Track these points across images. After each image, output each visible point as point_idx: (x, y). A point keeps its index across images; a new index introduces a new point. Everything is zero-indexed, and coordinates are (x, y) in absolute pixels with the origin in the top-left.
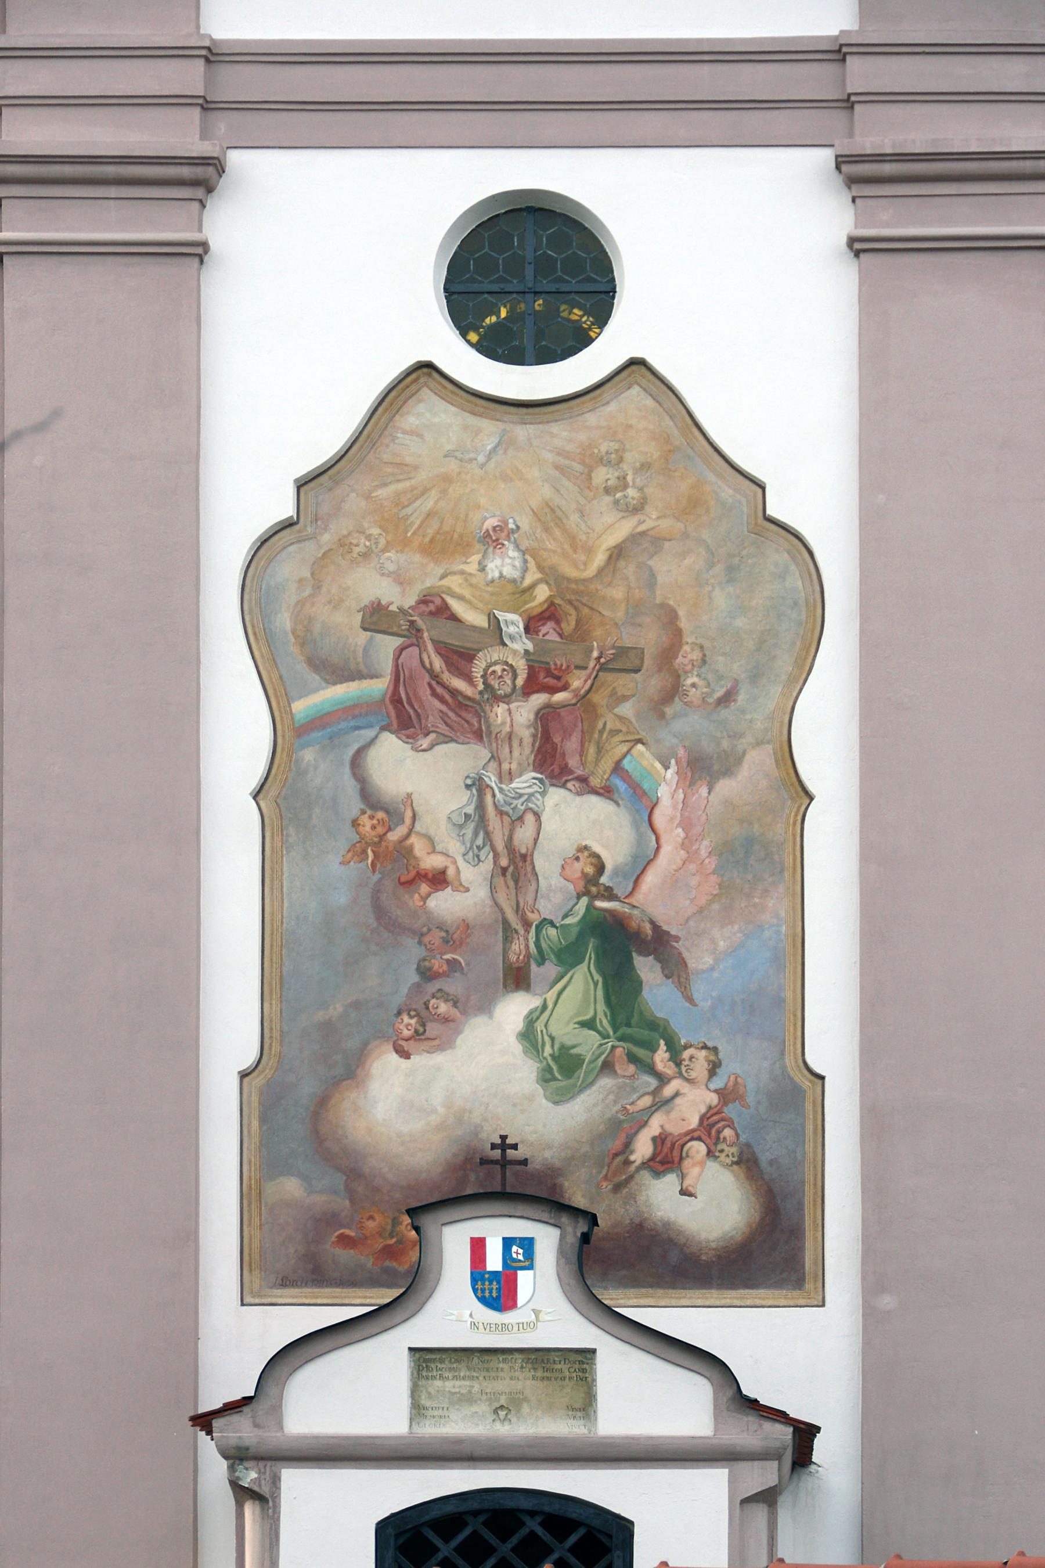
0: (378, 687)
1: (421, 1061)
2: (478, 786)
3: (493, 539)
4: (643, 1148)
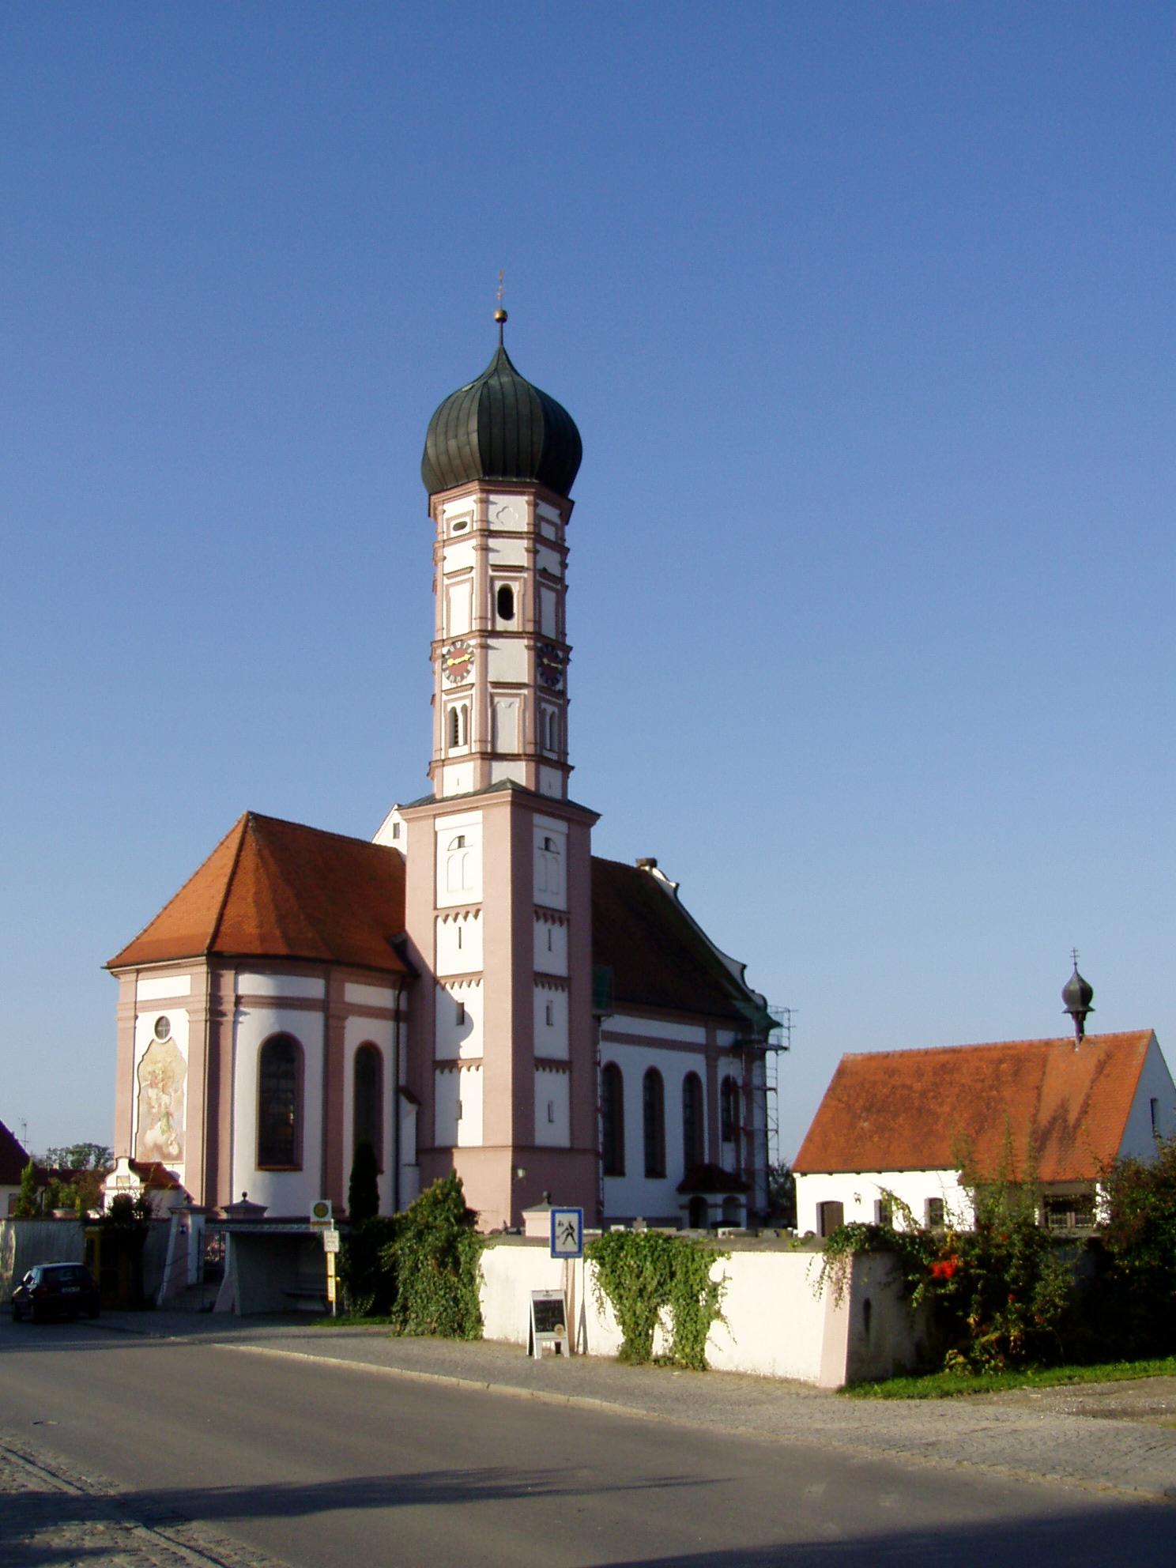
0: (149, 1082)
1: (152, 1131)
2: (157, 1095)
3: (160, 1061)
4: (169, 1142)
